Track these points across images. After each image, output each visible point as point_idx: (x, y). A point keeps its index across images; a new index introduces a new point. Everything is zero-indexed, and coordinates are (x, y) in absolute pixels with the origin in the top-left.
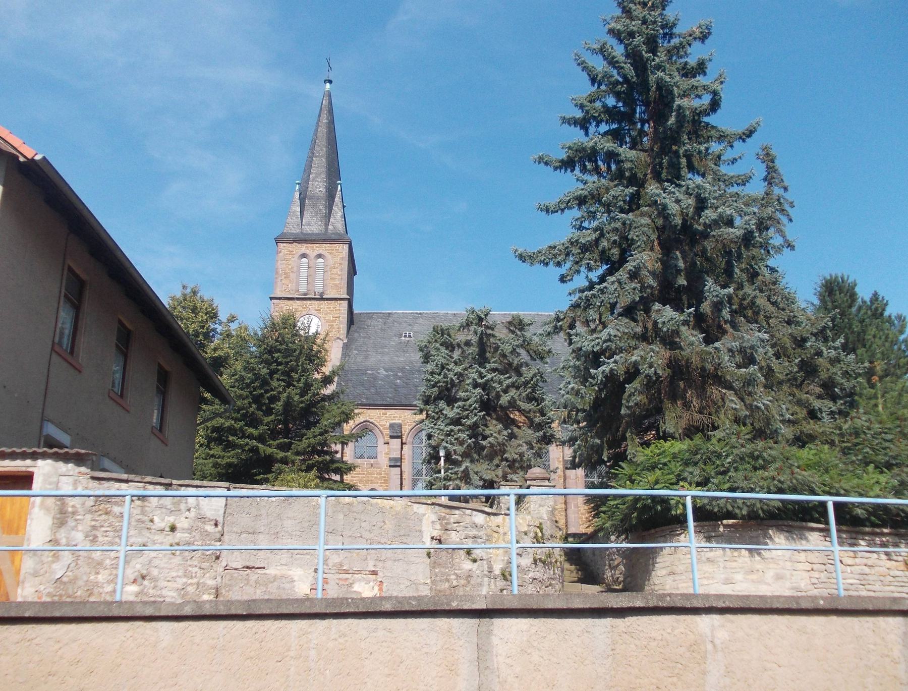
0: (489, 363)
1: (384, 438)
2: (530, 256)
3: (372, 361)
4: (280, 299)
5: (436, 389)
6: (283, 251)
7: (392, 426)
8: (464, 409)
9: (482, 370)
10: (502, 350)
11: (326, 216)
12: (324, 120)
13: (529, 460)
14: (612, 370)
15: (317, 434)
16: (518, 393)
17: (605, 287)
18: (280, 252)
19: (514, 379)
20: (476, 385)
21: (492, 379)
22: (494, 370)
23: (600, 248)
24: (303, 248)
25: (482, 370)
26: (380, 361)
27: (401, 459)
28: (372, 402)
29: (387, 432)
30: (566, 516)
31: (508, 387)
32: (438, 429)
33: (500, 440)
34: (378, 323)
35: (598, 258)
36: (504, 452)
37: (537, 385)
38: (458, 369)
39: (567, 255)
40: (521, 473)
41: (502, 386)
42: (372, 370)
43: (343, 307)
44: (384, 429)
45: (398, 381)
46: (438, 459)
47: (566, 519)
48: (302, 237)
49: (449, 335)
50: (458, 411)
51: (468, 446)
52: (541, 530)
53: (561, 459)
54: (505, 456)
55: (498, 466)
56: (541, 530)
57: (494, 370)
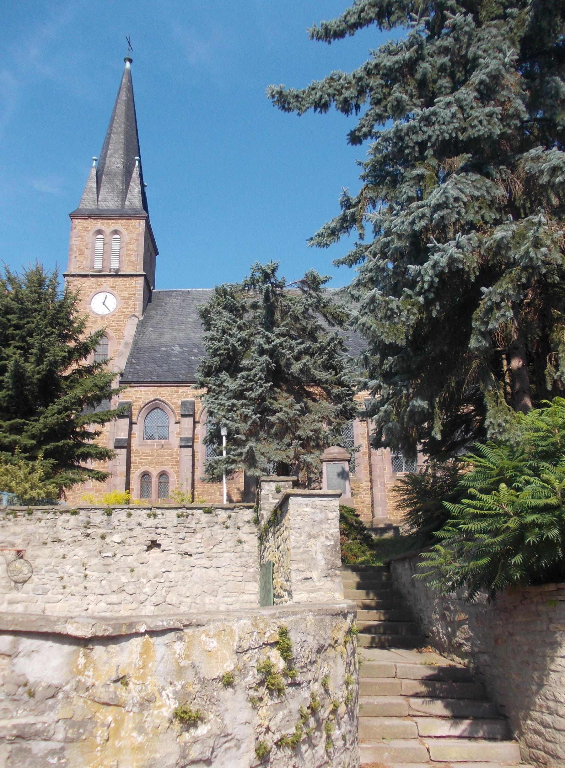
0: (278, 327)
1: (176, 417)
2: (297, 97)
3: (167, 338)
4: (73, 276)
5: (217, 358)
6: (77, 227)
7: (184, 404)
8: (248, 379)
9: (270, 335)
10: (293, 311)
11: (123, 192)
12: (124, 96)
13: (326, 437)
14: (452, 260)
15: (56, 411)
16: (313, 360)
17: (435, 114)
18: (75, 228)
19: (308, 343)
20: (262, 352)
21: (281, 345)
22: (282, 335)
23: (418, 76)
24: (99, 224)
25: (270, 335)
26: (175, 337)
27: (193, 438)
28: (163, 380)
29: (178, 411)
30: (372, 494)
31: (300, 353)
32: (220, 404)
33: (291, 415)
34: (177, 301)
35: (415, 92)
36: (297, 428)
37: (334, 351)
38: (243, 334)
39: (361, 92)
40: (317, 453)
41: (293, 351)
42: (166, 346)
43: (139, 284)
44: (175, 407)
45: (193, 358)
46: (220, 438)
47: (372, 498)
48: (98, 213)
49: (233, 297)
50: (241, 382)
51: (253, 423)
52: (286, 651)
53: (366, 435)
54: (298, 433)
55: (289, 445)
56: (286, 651)
57: (282, 335)
